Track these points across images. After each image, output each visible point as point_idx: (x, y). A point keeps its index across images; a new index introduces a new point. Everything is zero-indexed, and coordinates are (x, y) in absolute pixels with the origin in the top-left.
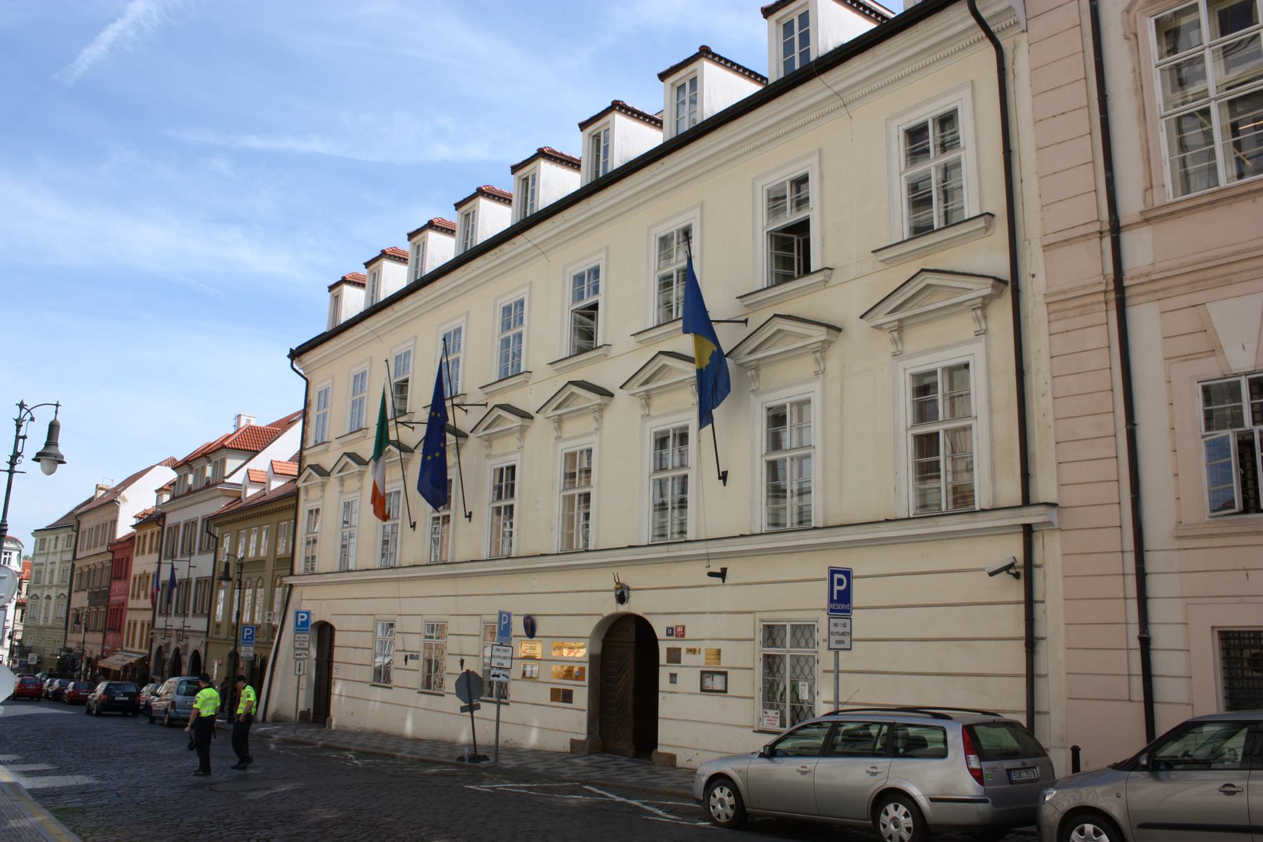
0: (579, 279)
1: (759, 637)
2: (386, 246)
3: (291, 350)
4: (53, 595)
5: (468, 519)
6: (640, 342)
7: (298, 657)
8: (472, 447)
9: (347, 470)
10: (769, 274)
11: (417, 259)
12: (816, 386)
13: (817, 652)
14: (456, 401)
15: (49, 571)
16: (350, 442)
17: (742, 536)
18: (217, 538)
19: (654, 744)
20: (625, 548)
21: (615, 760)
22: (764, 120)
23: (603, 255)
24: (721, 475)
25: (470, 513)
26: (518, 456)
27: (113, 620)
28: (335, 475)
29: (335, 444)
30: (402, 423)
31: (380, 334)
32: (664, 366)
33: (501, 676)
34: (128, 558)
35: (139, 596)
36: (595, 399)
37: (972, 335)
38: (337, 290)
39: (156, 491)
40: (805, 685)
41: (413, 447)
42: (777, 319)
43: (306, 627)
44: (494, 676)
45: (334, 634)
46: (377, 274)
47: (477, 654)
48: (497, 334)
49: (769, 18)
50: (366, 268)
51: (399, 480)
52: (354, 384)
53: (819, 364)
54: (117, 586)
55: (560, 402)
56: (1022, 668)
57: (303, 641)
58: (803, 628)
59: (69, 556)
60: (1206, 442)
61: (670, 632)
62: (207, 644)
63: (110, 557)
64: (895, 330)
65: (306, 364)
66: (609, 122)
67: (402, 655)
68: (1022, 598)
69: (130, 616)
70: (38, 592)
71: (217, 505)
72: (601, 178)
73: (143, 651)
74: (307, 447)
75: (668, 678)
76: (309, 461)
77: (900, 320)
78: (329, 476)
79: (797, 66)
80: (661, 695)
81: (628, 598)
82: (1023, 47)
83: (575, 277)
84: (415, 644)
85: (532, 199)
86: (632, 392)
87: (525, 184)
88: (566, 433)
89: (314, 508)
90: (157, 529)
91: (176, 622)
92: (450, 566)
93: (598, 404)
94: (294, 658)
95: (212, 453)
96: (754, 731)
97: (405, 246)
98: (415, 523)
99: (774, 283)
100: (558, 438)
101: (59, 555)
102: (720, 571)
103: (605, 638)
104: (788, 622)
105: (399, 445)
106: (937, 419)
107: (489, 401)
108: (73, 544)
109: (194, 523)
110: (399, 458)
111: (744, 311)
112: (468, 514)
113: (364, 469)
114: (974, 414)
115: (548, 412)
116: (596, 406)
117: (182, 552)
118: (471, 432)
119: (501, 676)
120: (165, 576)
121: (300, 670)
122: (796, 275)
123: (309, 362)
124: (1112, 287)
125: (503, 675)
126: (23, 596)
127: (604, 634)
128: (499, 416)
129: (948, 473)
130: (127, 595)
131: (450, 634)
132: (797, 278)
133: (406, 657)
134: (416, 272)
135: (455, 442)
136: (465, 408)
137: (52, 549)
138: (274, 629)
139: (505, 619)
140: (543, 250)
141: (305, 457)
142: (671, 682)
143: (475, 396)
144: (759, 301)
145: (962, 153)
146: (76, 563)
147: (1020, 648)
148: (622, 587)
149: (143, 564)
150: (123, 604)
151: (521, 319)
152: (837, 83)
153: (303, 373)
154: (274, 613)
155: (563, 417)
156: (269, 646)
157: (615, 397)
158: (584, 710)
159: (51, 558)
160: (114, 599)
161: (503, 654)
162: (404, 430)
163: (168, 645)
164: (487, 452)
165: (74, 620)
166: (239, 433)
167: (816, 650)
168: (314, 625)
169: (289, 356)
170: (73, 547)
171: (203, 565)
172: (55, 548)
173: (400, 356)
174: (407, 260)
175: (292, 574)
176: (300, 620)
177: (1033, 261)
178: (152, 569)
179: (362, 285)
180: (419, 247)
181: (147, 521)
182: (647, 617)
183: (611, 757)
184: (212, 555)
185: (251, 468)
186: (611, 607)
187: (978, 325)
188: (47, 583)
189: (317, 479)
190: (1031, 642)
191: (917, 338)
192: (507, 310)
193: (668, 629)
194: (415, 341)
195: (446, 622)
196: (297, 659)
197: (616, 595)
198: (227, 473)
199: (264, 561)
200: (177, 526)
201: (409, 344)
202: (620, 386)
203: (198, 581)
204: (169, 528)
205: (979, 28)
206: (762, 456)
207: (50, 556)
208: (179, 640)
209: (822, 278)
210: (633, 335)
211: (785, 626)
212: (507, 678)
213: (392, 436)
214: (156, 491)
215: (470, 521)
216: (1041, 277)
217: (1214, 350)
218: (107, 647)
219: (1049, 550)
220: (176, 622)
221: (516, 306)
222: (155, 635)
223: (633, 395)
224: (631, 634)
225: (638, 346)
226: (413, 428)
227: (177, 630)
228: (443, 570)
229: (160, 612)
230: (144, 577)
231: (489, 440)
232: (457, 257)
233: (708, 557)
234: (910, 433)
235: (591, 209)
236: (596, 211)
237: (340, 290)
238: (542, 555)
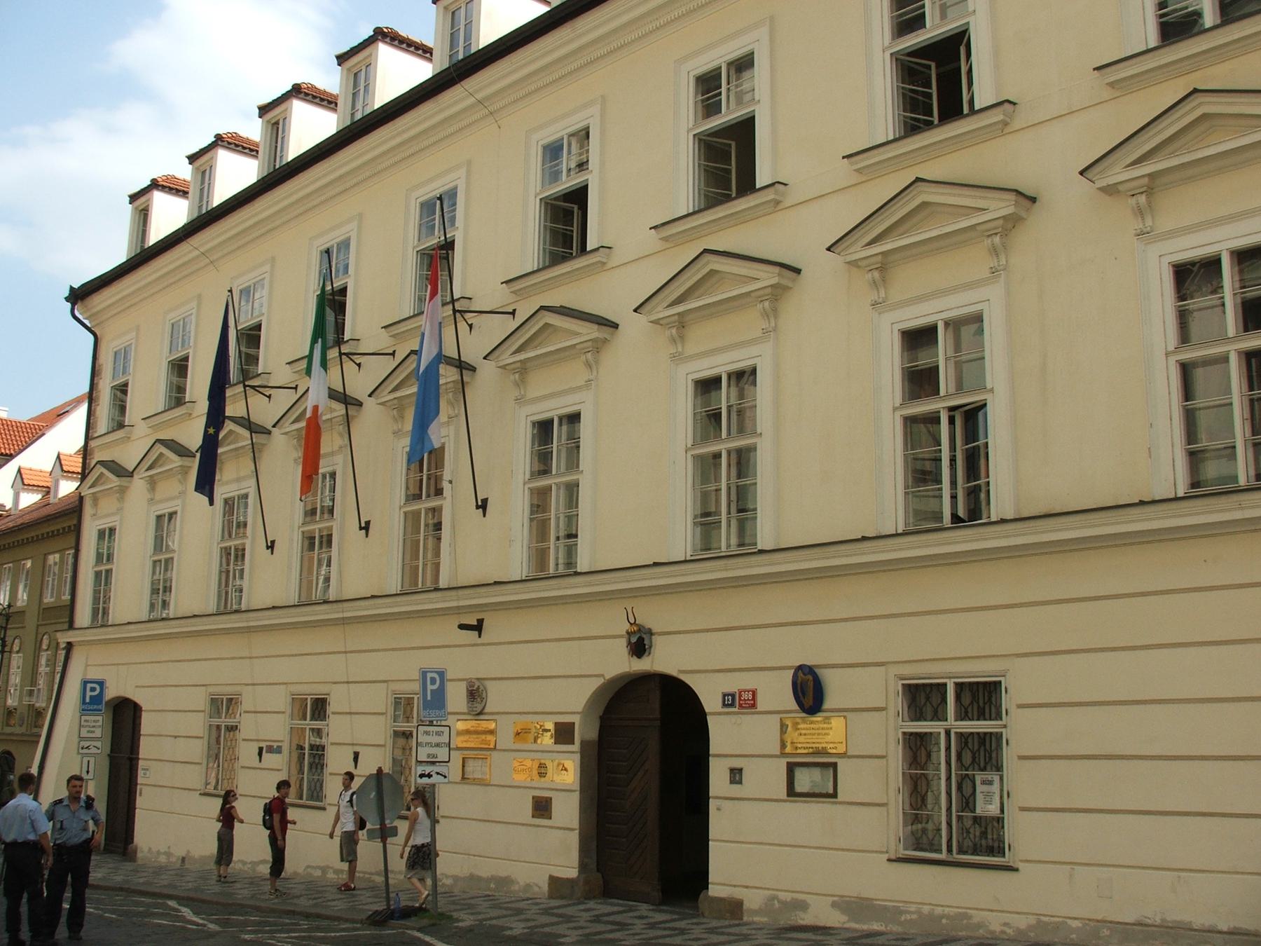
0: (553, 151)
1: (897, 703)
2: (158, 173)
3: (72, 288)
5: (364, 531)
6: (665, 239)
7: (85, 751)
10: (541, 252)
11: (202, 190)
13: (1005, 726)
14: (345, 349)
17: (864, 539)
19: (700, 877)
20: (368, 598)
21: (631, 911)
23: (354, 225)
24: (480, 503)
25: (368, 523)
30: (253, 387)
31: (215, 257)
32: (712, 273)
33: (435, 776)
36: (589, 332)
37: (759, 333)
38: (143, 199)
40: (990, 783)
42: (708, 257)
43: (98, 704)
44: (422, 776)
45: (140, 717)
46: (208, 172)
47: (382, 743)
48: (312, 289)
49: (438, 3)
50: (339, 65)
52: (115, 364)
53: (997, 255)
57: (94, 727)
58: (928, 690)
61: (730, 700)
64: (877, 268)
65: (95, 310)
74: (96, 435)
75: (727, 776)
76: (98, 456)
77: (1150, 175)
78: (132, 476)
80: (713, 804)
81: (650, 647)
83: (545, 148)
84: (277, 728)
85: (282, 150)
86: (654, 318)
87: (275, 128)
88: (159, 495)
92: (335, 606)
93: (772, 286)
94: (79, 753)
96: (889, 860)
97: (185, 172)
98: (273, 542)
99: (547, 264)
100: (151, 501)
102: (476, 623)
103: (604, 714)
104: (950, 678)
105: (247, 423)
106: (938, 393)
110: (250, 442)
112: (363, 525)
113: (126, 484)
114: (989, 386)
115: (503, 357)
116: (179, 468)
118: (274, 426)
119: (435, 776)
121: (88, 772)
122: (936, 122)
123: (99, 308)
125: (438, 773)
127: (603, 708)
128: (161, 454)
129: (732, 503)
131: (333, 713)
132: (937, 126)
133: (261, 750)
135: (344, 412)
136: (358, 359)
138: (39, 714)
139: (433, 681)
140: (491, 109)
141: (92, 450)
142: (731, 782)
144: (736, 213)
145: (589, 177)
148: (639, 630)
151: (346, 267)
153: (89, 325)
154: (39, 690)
155: (528, 365)
156: (35, 739)
157: (620, 327)
158: (573, 830)
161: (435, 739)
162: (256, 400)
164: (395, 428)
167: (1003, 722)
168: (108, 703)
169: (67, 299)
174: (187, 193)
175: (71, 626)
176: (89, 694)
179: (183, 193)
182: (683, 677)
183: (626, 905)
185: (24, 465)
186: (621, 663)
187: (876, 292)
189: (113, 481)
191: (701, 336)
193: (724, 695)
194: (273, 266)
195: (328, 694)
196: (84, 755)
197: (629, 643)
202: (484, 355)
209: (1001, 117)
210: (655, 228)
211: (945, 685)
212: (445, 777)
215: (272, 553)
224: (653, 706)
225: (1107, 94)
226: (269, 397)
228: (322, 613)
232: (263, 178)
233: (458, 610)
234: (301, 529)
235: (441, 111)
236: (584, 40)
237: (149, 200)
238: (496, 583)
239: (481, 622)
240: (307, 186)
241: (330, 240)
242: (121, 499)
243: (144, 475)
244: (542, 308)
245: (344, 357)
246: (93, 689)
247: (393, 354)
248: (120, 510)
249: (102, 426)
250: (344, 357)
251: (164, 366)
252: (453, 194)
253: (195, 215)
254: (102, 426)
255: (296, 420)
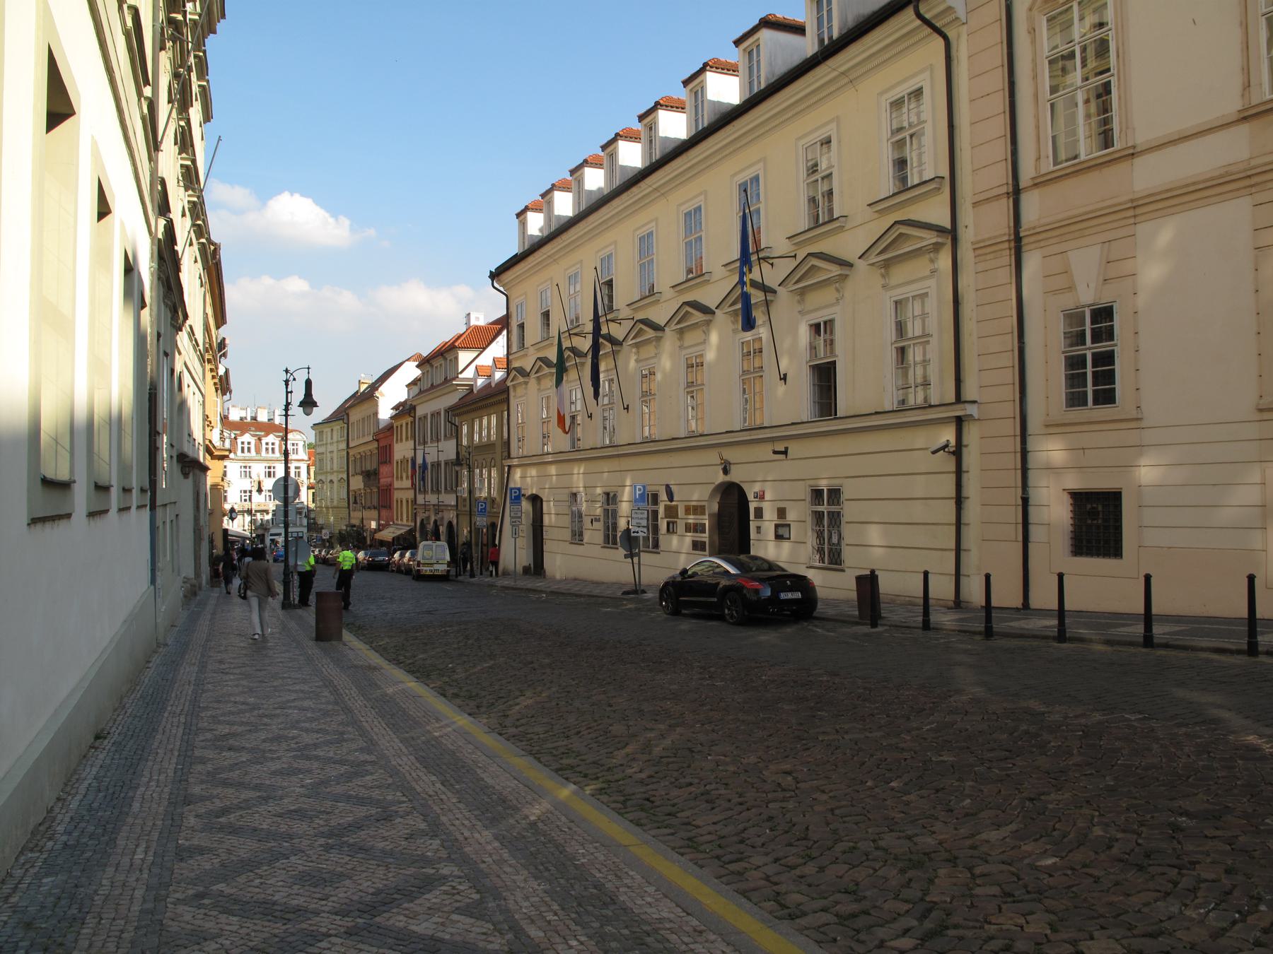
4: (335, 479)
6: (730, 271)
8: (784, 300)
9: (685, 321)
11: (696, 107)
12: (932, 283)
15: (329, 459)
16: (544, 348)
18: (457, 427)
22: (788, 99)
25: (628, 406)
26: (836, 309)
27: (384, 501)
28: (533, 376)
29: (532, 350)
32: (901, 235)
34: (390, 445)
35: (402, 478)
36: (835, 270)
37: (928, 273)
39: (407, 386)
41: (662, 324)
42: (898, 226)
48: (802, 180)
51: (575, 380)
54: (384, 470)
55: (680, 316)
56: (953, 519)
59: (343, 446)
60: (1065, 357)
62: (457, 515)
63: (375, 445)
66: (702, 81)
67: (590, 518)
68: (954, 469)
69: (397, 495)
70: (323, 478)
71: (452, 399)
72: (828, 45)
73: (410, 523)
76: (516, 364)
79: (826, 42)
82: (964, 38)
89: (821, 320)
90: (410, 419)
91: (432, 499)
93: (933, 244)
95: (446, 352)
100: (681, 347)
101: (335, 444)
107: (798, 252)
108: (346, 435)
109: (439, 413)
111: (793, 248)
116: (883, 262)
117: (432, 439)
120: (419, 461)
124: (1012, 237)
126: (312, 480)
128: (687, 312)
130: (393, 476)
131: (847, 500)
134: (651, 154)
135: (764, 298)
136: (771, 261)
137: (329, 441)
140: (851, 77)
143: (625, 312)
145: (761, 205)
146: (350, 451)
147: (952, 504)
149: (402, 450)
150: (390, 485)
152: (841, 65)
159: (330, 448)
160: (383, 481)
161: (640, 516)
163: (428, 518)
165: (353, 500)
166: (469, 331)
170: (345, 438)
171: (448, 450)
172: (332, 439)
173: (644, 237)
176: (513, 495)
177: (967, 216)
178: (410, 454)
180: (696, 93)
181: (404, 410)
182: (742, 485)
184: (454, 441)
186: (721, 478)
188: (329, 470)
190: (959, 500)
192: (688, 215)
198: (461, 368)
199: (494, 444)
200: (425, 417)
201: (700, 198)
203: (446, 463)
204: (420, 419)
205: (925, 27)
206: (807, 363)
207: (329, 446)
208: (436, 514)
213: (604, 331)
214: (407, 386)
216: (971, 230)
217: (1071, 288)
218: (382, 522)
219: (972, 435)
220: (432, 499)
221: (751, 183)
222: (418, 510)
223: (872, 264)
227: (434, 505)
229: (420, 490)
230: (404, 461)
231: (681, 332)
233: (772, 440)
234: (894, 346)
236: (693, 162)
239: (787, 449)
240: (705, 151)
241: (746, 176)
242: (526, 388)
243: (793, 288)
244: (896, 222)
245: (761, 261)
246: (515, 492)
247: (795, 256)
248: (526, 393)
249: (514, 349)
250: (761, 261)
251: (539, 317)
252: (699, 208)
253: (693, 132)
254: (514, 349)
255: (733, 304)
